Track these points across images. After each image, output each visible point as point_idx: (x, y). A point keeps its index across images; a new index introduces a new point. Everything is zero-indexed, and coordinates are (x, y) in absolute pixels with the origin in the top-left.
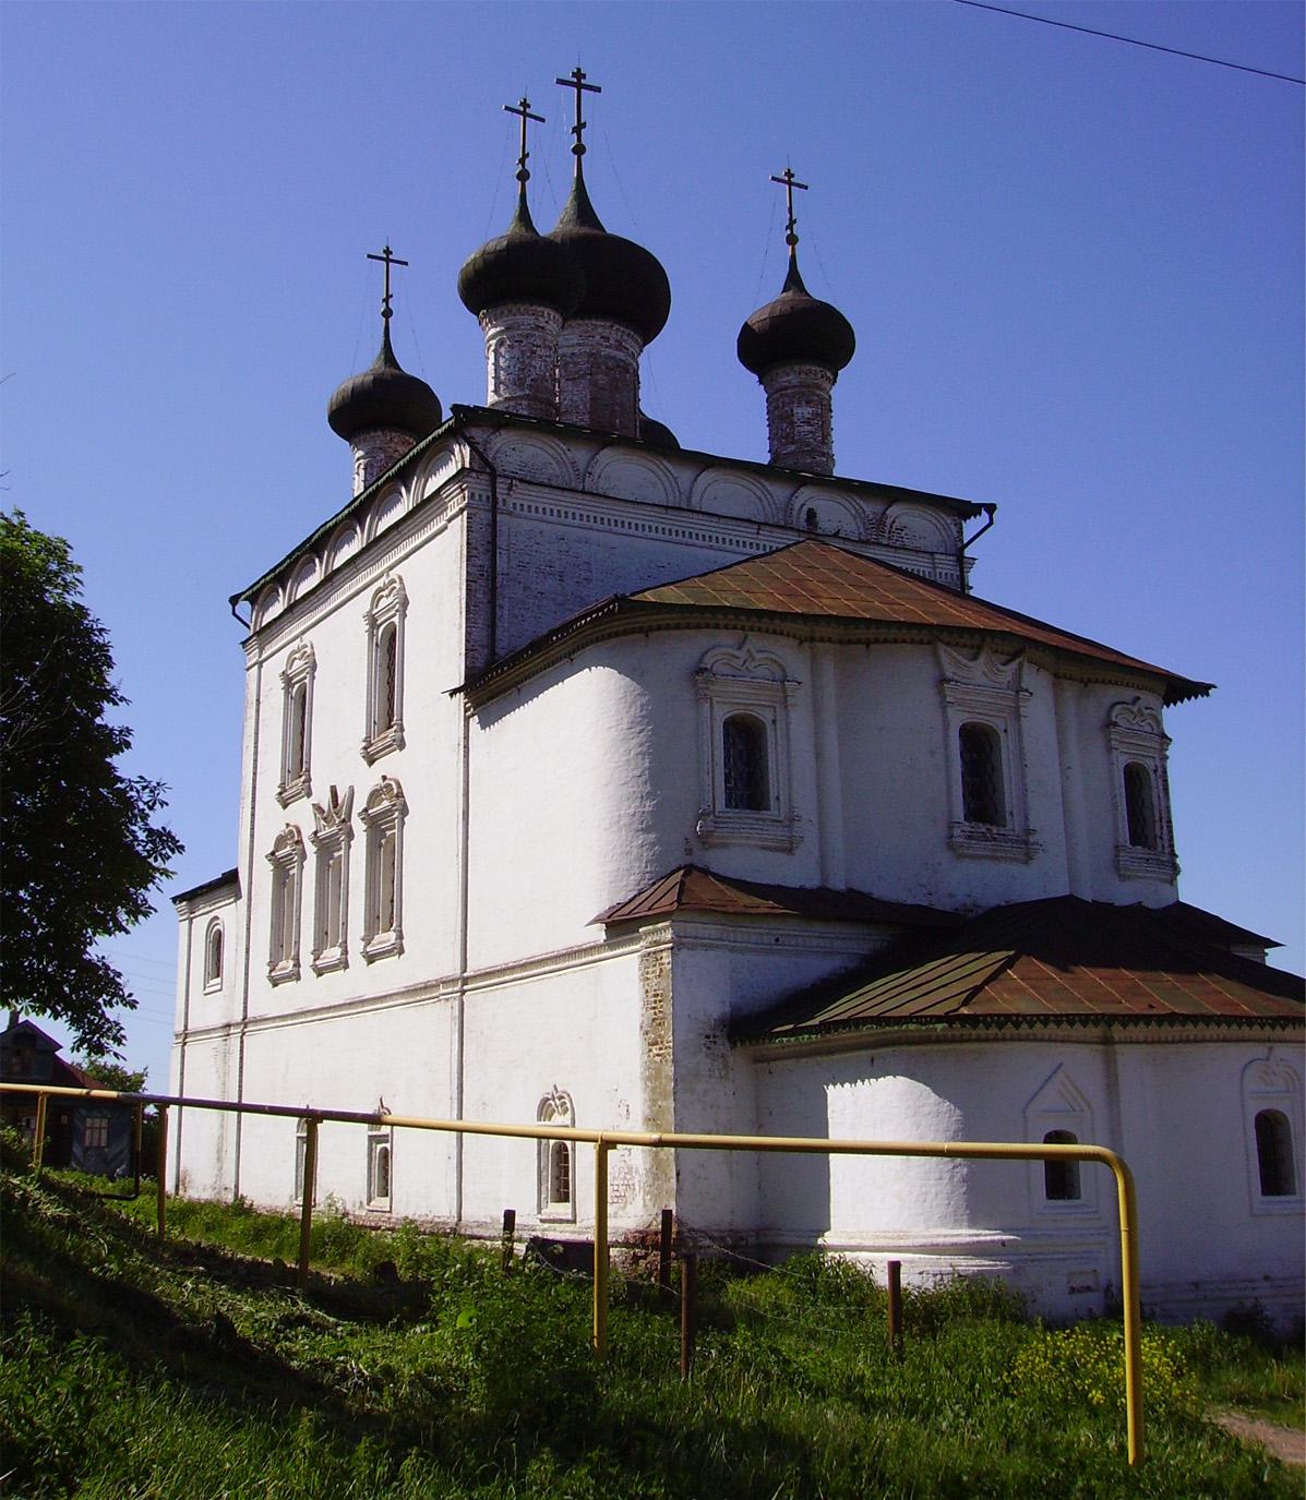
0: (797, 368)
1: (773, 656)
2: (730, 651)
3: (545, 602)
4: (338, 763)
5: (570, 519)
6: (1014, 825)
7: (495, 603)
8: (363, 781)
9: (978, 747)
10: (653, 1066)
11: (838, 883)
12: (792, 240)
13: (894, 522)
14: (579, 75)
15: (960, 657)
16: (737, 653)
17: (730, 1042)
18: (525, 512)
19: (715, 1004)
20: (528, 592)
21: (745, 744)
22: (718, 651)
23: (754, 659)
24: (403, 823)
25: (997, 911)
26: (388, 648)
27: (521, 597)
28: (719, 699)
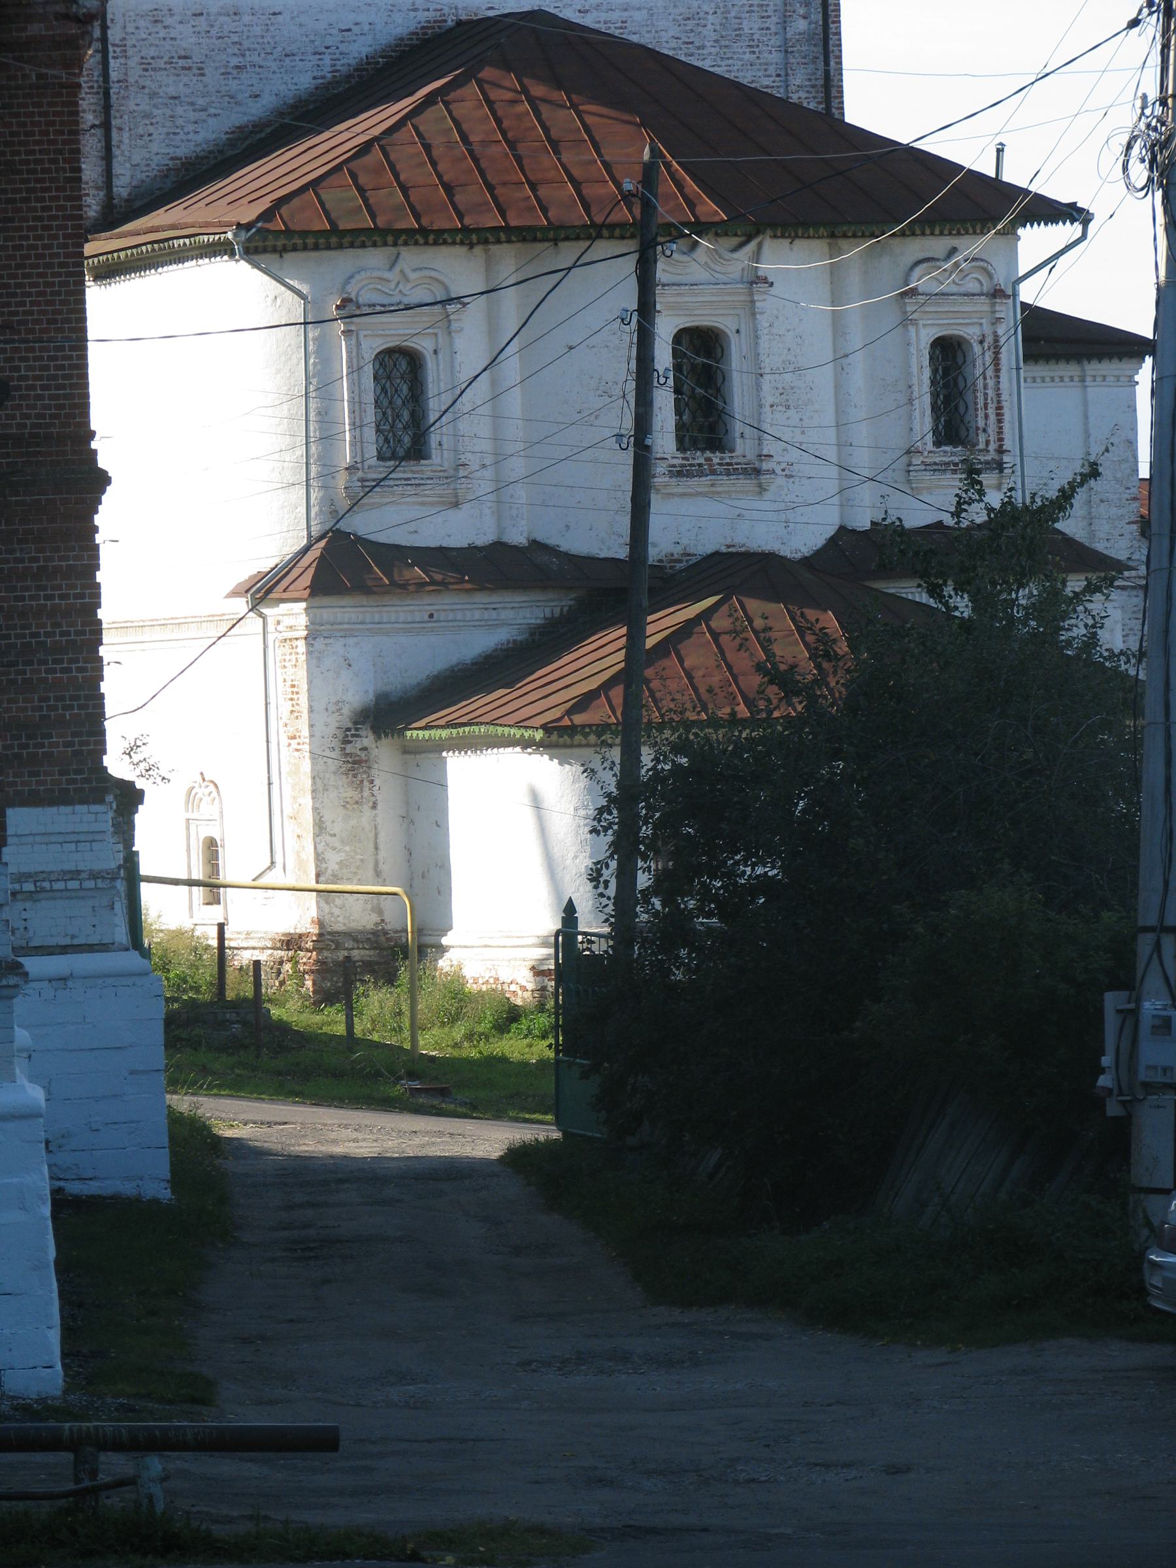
1: (433, 274)
3: (180, 110)
6: (743, 449)
7: (110, 123)
10: (293, 761)
11: (517, 537)
16: (387, 275)
17: (374, 732)
20: (156, 101)
21: (400, 382)
23: (408, 280)
25: (716, 557)
27: (147, 108)
28: (365, 333)
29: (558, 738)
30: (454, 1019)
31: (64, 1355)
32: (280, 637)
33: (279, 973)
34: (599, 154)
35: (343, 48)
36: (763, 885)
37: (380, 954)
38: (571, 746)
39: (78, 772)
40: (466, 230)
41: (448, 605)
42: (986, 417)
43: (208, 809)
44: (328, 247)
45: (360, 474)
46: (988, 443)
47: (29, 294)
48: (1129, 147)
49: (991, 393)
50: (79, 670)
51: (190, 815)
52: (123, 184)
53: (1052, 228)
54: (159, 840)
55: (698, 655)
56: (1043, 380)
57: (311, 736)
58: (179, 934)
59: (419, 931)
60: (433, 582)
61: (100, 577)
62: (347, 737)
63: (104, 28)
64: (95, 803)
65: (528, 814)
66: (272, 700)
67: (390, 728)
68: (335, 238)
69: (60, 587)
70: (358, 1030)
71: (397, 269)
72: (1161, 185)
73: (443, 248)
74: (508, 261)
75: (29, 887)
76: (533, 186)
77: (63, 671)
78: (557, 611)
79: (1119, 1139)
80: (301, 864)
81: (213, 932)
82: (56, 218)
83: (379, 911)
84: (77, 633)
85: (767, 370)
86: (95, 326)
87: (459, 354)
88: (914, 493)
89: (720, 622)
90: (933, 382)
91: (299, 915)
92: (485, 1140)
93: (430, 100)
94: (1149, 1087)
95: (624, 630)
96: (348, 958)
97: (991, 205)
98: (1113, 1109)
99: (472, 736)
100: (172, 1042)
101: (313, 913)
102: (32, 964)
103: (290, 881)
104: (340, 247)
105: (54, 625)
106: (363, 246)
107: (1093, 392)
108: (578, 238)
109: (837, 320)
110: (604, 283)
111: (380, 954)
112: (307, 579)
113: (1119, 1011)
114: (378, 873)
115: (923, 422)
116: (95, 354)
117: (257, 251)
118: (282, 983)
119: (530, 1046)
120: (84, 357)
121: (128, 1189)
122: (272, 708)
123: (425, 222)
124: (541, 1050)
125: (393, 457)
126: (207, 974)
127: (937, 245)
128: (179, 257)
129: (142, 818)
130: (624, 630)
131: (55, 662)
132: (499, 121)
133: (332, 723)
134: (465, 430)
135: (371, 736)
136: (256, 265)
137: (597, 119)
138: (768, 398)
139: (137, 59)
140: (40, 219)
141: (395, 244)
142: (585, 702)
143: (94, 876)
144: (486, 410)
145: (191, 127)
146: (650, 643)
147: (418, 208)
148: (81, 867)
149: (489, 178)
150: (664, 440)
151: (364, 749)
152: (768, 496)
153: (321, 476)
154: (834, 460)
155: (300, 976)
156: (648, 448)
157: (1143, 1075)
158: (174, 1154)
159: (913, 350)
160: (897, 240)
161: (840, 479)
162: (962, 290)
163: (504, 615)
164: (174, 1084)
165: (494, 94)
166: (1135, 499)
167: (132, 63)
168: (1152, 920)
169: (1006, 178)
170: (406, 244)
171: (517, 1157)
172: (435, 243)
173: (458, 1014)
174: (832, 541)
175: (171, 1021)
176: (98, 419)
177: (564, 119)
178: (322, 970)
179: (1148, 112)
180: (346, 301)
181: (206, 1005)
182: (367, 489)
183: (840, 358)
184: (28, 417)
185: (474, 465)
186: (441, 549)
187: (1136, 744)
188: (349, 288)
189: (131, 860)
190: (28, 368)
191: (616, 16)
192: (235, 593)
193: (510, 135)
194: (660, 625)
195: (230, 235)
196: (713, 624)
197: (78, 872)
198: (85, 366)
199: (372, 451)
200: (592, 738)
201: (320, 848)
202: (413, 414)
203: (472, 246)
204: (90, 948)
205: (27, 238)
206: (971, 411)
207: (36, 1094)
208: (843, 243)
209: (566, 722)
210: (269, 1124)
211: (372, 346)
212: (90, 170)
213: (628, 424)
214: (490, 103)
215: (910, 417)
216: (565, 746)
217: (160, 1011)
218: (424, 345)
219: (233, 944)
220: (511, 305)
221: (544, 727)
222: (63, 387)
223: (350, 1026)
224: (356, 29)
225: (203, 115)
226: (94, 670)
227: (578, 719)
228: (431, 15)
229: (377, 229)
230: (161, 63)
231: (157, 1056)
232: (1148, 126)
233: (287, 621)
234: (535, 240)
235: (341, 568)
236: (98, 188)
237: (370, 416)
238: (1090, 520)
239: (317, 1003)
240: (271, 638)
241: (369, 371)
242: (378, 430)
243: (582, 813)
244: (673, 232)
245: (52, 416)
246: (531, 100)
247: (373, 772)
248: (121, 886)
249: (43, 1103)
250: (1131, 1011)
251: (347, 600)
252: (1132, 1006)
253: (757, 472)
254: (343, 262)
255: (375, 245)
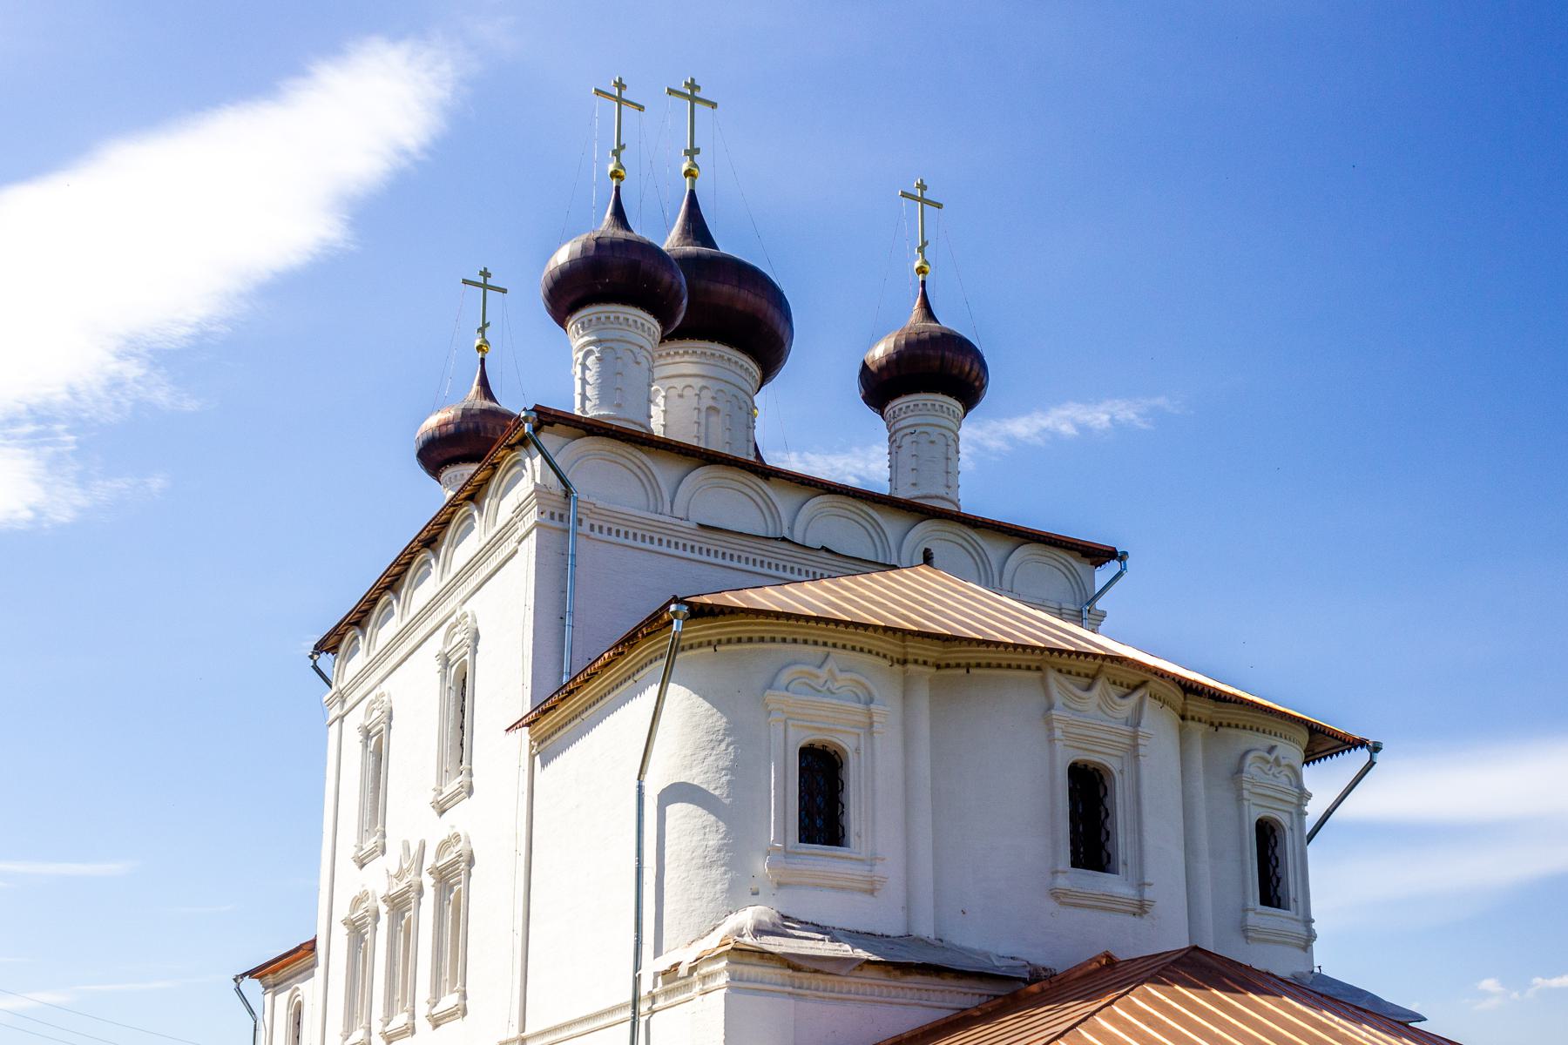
4: (413, 820)
8: (435, 830)
9: (1088, 791)
14: (693, 86)
15: (1071, 687)
22: (798, 668)
24: (469, 875)
26: (460, 688)
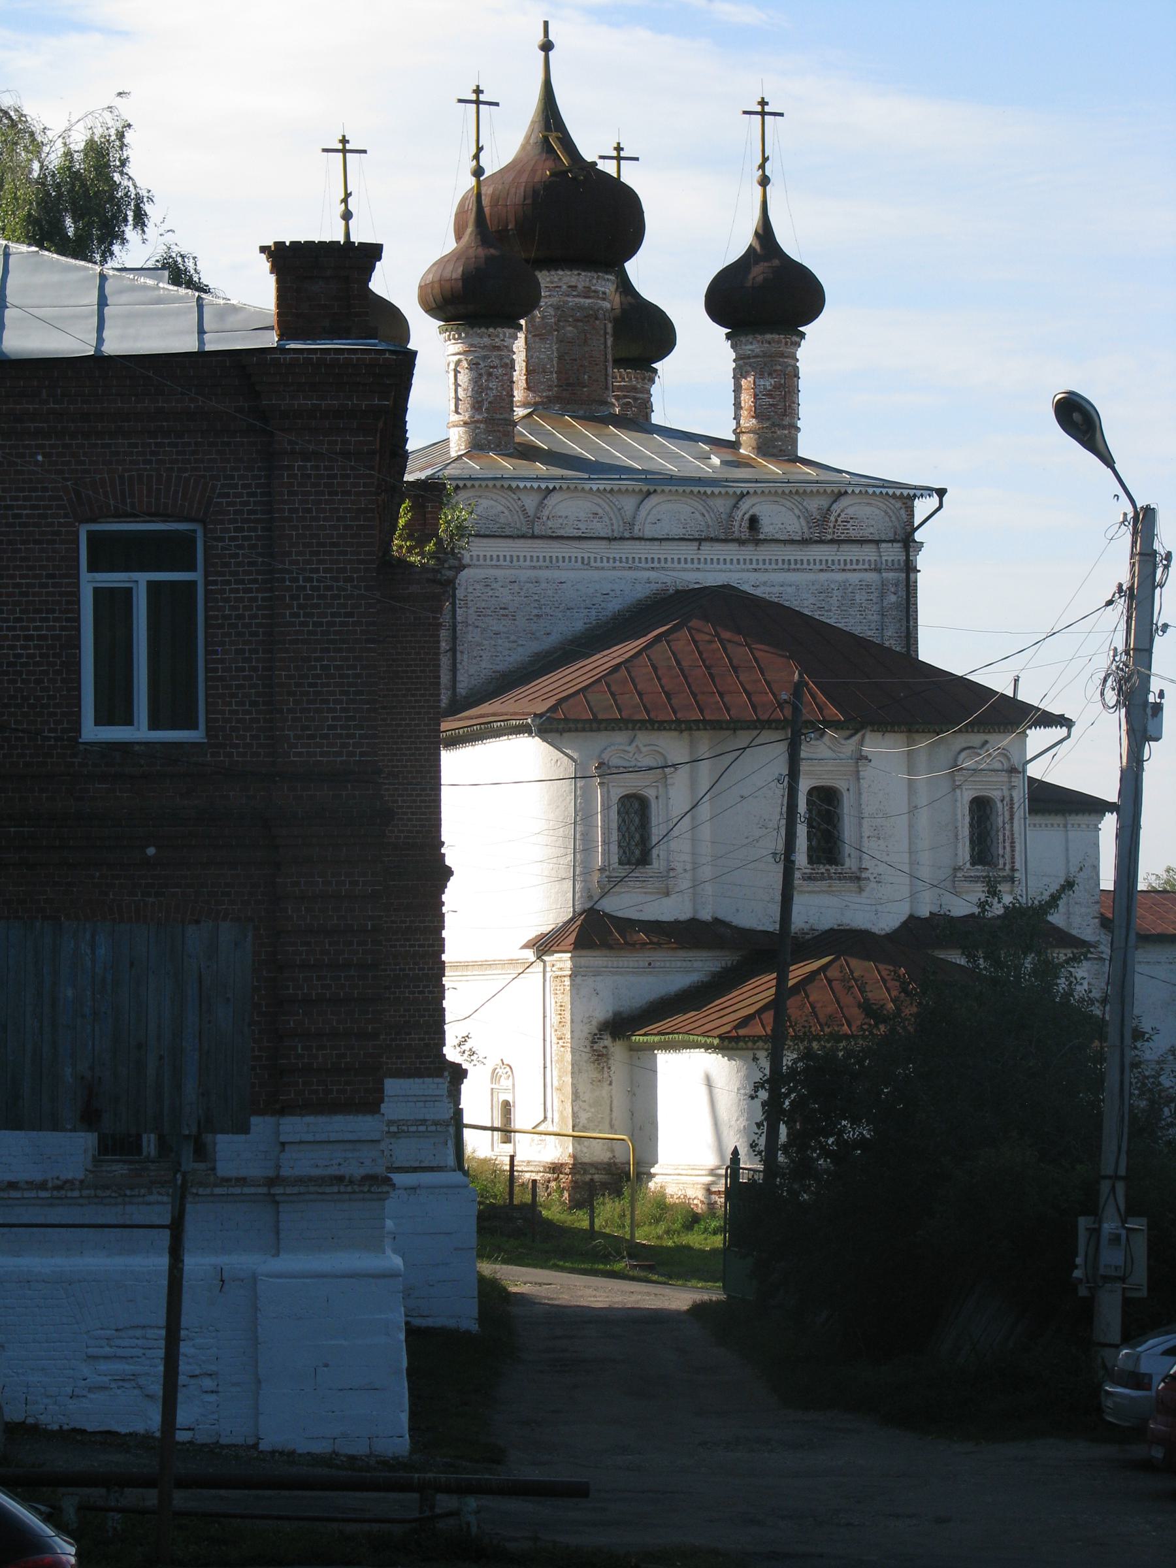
0: (759, 337)
2: (621, 747)
3: (500, 641)
5: (521, 562)
6: (850, 864)
11: (706, 915)
12: (764, 181)
13: (839, 515)
16: (628, 748)
18: (482, 562)
19: (602, 1011)
29: (728, 1044)
30: (658, 1221)
31: (410, 1430)
32: (554, 974)
33: (548, 1187)
34: (763, 675)
35: (603, 605)
36: (862, 1143)
37: (609, 1175)
38: (737, 1049)
39: (428, 1057)
40: (678, 722)
41: (661, 958)
42: (1004, 848)
43: (505, 1083)
44: (591, 730)
45: (607, 873)
46: (1005, 864)
47: (405, 755)
48: (1105, 680)
49: (1007, 833)
50: (430, 992)
51: (494, 1086)
52: (463, 687)
53: (1048, 730)
54: (475, 1102)
55: (819, 994)
56: (1052, 825)
57: (572, 1038)
58: (485, 1161)
59: (637, 1164)
60: (651, 943)
61: (444, 934)
62: (594, 1039)
63: (454, 589)
64: (437, 1077)
65: (703, 1090)
66: (548, 1014)
67: (619, 1037)
68: (595, 724)
69: (419, 940)
70: (596, 1228)
71: (634, 745)
72: (1125, 705)
73: (663, 732)
74: (705, 743)
75: (394, 1129)
76: (721, 695)
77: (420, 992)
78: (729, 963)
79: (1087, 1311)
80: (562, 1118)
81: (507, 1160)
82: (423, 707)
83: (612, 1151)
84: (429, 969)
85: (866, 815)
86: (446, 776)
87: (672, 800)
88: (957, 894)
89: (833, 973)
90: (971, 825)
91: (558, 1151)
92: (677, 1298)
93: (658, 639)
94: (1106, 1279)
95: (775, 975)
96: (592, 1180)
97: (1012, 715)
98: (1083, 1292)
99: (673, 1041)
100: (481, 1230)
101: (571, 1150)
102: (397, 1178)
103: (556, 1129)
104: (599, 730)
105: (415, 964)
106: (613, 729)
107: (1072, 835)
108: (748, 728)
109: (911, 784)
110: (767, 759)
111: (609, 1175)
112: (572, 938)
113: (1087, 1229)
114: (612, 1126)
115: (964, 852)
116: (446, 794)
117: (546, 731)
118: (549, 1195)
119: (706, 1239)
120: (438, 795)
121: (451, 1323)
122: (548, 1019)
123: (652, 715)
124: (718, 1241)
125: (629, 863)
126: (501, 1187)
127: (976, 739)
128: (497, 733)
129: (466, 1087)
130: (775, 975)
131: (415, 987)
132: (700, 653)
133: (586, 1030)
134: (675, 849)
135: (610, 1040)
136: (544, 740)
137: (762, 654)
138: (866, 834)
139: (473, 609)
140: (414, 707)
141: (633, 729)
142: (746, 1021)
143: (436, 1123)
144: (688, 835)
145: (507, 653)
146: (790, 983)
147: (648, 706)
148: (428, 1117)
149: (693, 688)
150: (801, 858)
151: (605, 1047)
152: (864, 894)
153: (582, 874)
154: (906, 869)
155: (561, 1191)
156: (793, 862)
157: (1102, 1271)
158: (480, 1302)
159: (959, 804)
160: (958, 736)
161: (911, 885)
162: (991, 767)
163: (696, 964)
164: (481, 1256)
165: (700, 637)
166: (1097, 903)
167: (471, 611)
168: (1109, 1171)
169: (1021, 697)
170: (640, 729)
171: (698, 1310)
172: (659, 729)
173: (661, 1217)
174: (905, 924)
175: (481, 1217)
176: (447, 833)
177: (742, 653)
178: (575, 1186)
179: (1117, 659)
180: (601, 764)
181: (501, 1207)
182: (611, 883)
183: (913, 810)
184: (403, 831)
185: (680, 870)
186: (657, 922)
187: (1101, 1058)
188: (604, 756)
189: (459, 1113)
190: (404, 801)
191: (776, 589)
192: (526, 946)
193: (707, 663)
194: (797, 972)
195: (529, 721)
196: (829, 974)
197: (426, 1120)
198: (439, 801)
199: (615, 859)
200: (750, 1044)
201: (576, 1109)
202: (642, 837)
203: (681, 731)
204: (431, 1169)
205: (405, 719)
206: (995, 844)
207: (397, 1262)
208: (917, 736)
209: (734, 1033)
210: (540, 1284)
211: (617, 793)
212: (445, 678)
213: (781, 846)
214: (695, 642)
215: (956, 848)
216: (732, 1049)
217: (474, 1210)
218: (650, 793)
219: (519, 1169)
220: (705, 772)
221: (719, 1036)
222: (424, 813)
223: (592, 1223)
224: (612, 594)
225: (514, 645)
226: (439, 992)
227: (742, 1032)
228: (659, 586)
229: (758, 720)
230: (489, 612)
231: (473, 1240)
232: (1118, 667)
233: (559, 965)
234: (722, 729)
235: (592, 932)
236: (447, 689)
237: (615, 836)
238: (1069, 914)
239: (571, 1208)
240: (548, 975)
241: (615, 808)
242: (619, 846)
243: (742, 1091)
244: (811, 725)
245: (417, 832)
246: (721, 641)
247: (611, 1062)
248: (452, 1130)
249: (402, 1268)
250: (1094, 1229)
251: (597, 953)
252: (1096, 1226)
253: (859, 879)
254: (600, 740)
255: (620, 729)
